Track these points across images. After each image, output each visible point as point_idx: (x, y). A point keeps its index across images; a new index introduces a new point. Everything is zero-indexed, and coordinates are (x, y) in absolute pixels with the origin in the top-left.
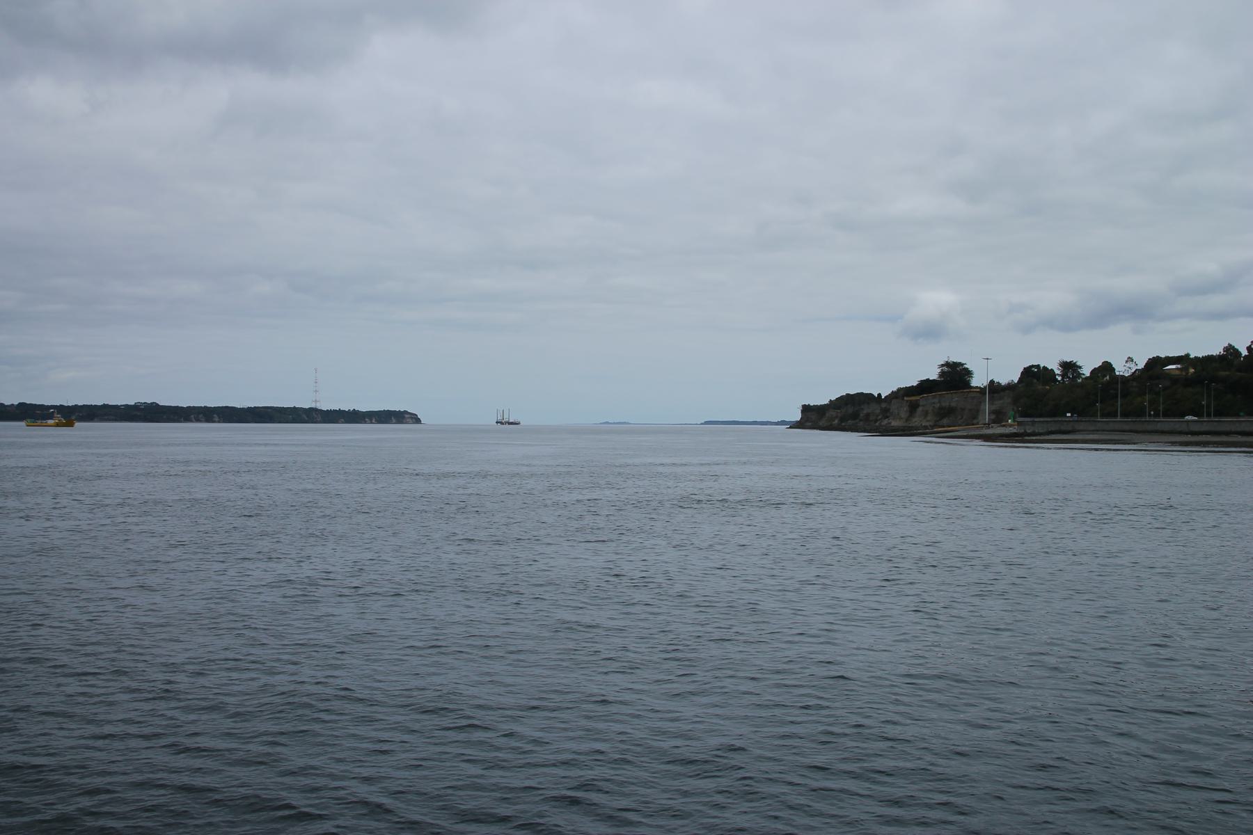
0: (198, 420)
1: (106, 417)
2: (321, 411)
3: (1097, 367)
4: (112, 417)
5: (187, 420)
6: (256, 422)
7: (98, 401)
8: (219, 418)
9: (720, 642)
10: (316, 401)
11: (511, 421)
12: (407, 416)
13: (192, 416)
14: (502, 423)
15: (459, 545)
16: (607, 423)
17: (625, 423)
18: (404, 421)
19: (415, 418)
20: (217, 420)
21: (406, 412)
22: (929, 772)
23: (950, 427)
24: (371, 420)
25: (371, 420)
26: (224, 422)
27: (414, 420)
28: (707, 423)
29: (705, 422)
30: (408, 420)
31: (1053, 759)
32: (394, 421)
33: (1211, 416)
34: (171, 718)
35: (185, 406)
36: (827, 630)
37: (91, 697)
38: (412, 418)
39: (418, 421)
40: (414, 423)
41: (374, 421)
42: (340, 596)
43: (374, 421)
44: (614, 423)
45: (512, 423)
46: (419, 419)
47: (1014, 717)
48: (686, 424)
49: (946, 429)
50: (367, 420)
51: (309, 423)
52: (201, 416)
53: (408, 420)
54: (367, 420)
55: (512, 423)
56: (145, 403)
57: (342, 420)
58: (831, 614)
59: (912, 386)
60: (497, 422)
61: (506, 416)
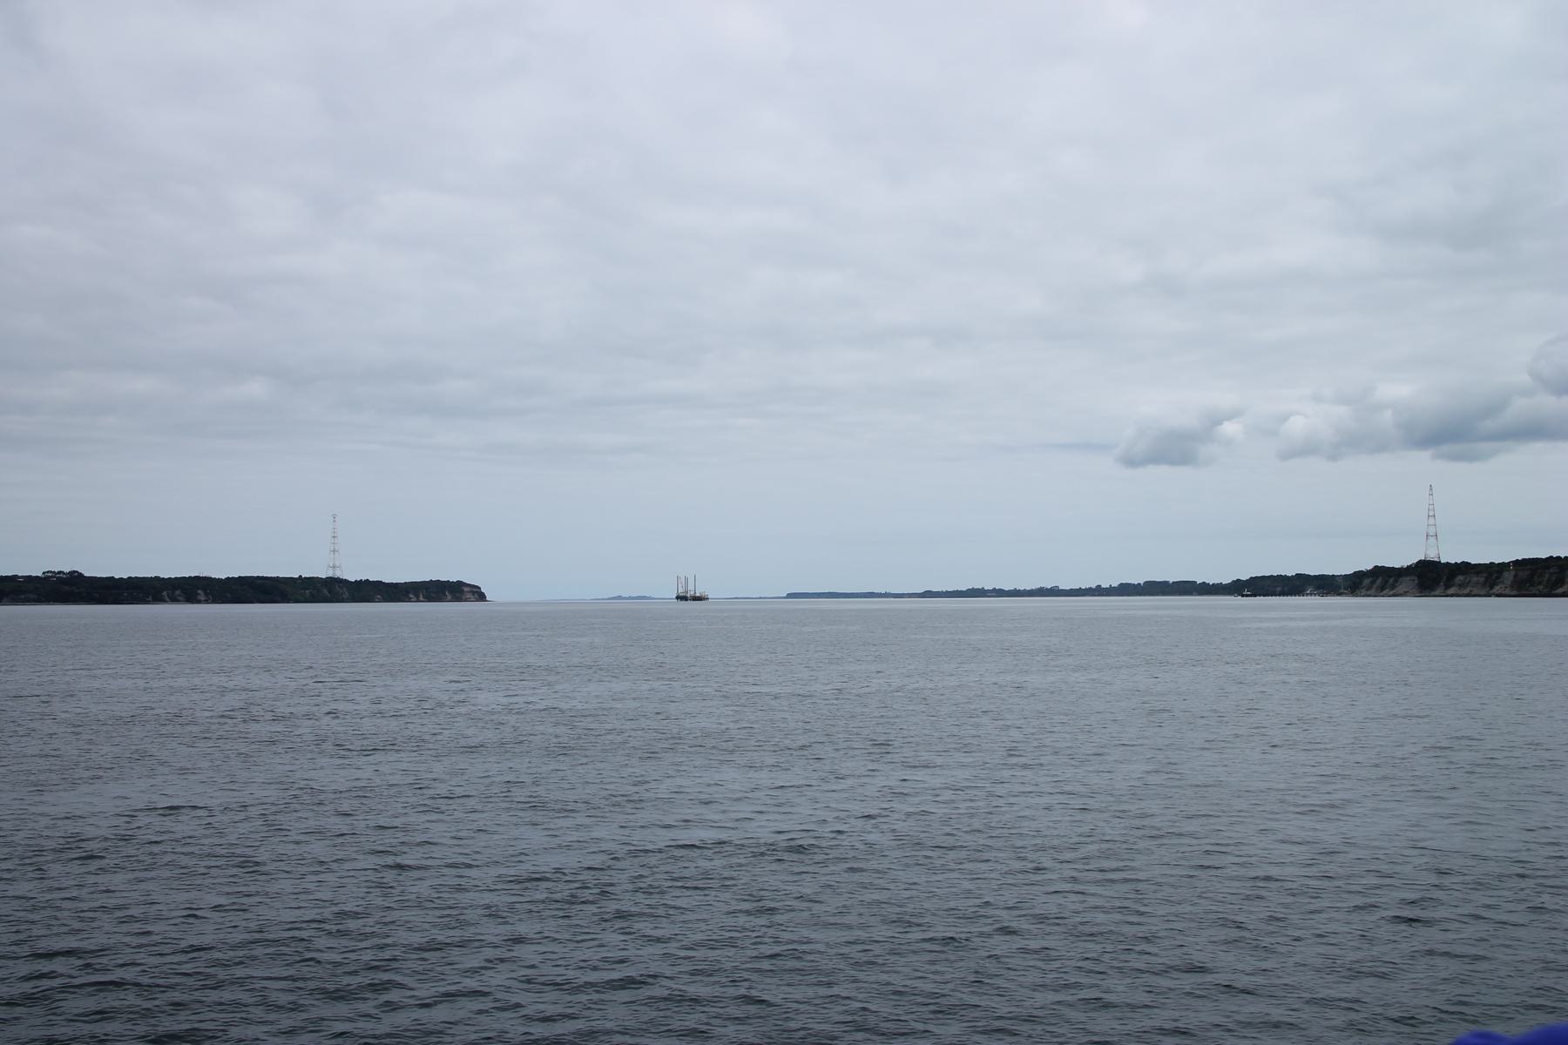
0: (174, 600)
1: (22, 596)
3: (371, 580)
4: (32, 596)
5: (158, 599)
6: (1128, 595)
8: (206, 594)
10: (334, 567)
11: (698, 595)
12: (466, 589)
13: (165, 593)
16: (620, 597)
18: (464, 598)
19: (477, 592)
20: (203, 598)
21: (460, 584)
22: (979, 1009)
24: (417, 597)
25: (417, 597)
26: (214, 601)
27: (477, 596)
28: (790, 596)
29: (788, 594)
31: (525, 797)
35: (117, 577)
36: (676, 792)
38: (473, 593)
39: (481, 597)
41: (421, 599)
43: (421, 599)
44: (630, 598)
46: (484, 594)
48: (760, 598)
52: (178, 592)
53: (468, 596)
56: (60, 572)
57: (379, 596)
60: (678, 598)
61: (691, 587)
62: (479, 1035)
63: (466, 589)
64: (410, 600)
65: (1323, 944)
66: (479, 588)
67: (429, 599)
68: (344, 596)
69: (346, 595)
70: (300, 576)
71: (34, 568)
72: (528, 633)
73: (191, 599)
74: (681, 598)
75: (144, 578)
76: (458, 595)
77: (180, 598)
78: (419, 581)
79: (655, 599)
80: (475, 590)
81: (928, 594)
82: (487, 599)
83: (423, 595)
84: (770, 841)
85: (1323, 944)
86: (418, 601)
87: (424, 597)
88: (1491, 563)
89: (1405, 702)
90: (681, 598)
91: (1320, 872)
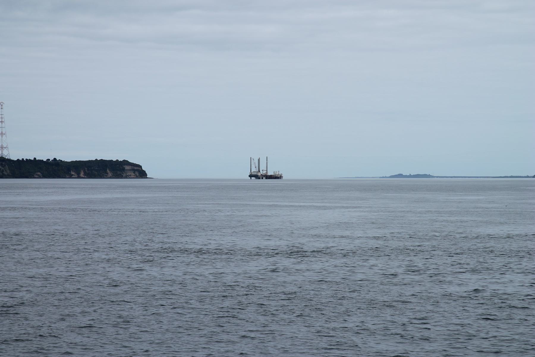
2: (9, 160)
5: (523, 178)
7: (44, 156)
9: (194, 352)
11: (270, 173)
12: (127, 168)
14: (257, 177)
15: (347, 299)
16: (400, 176)
17: (425, 176)
18: (124, 175)
19: (137, 170)
21: (125, 162)
30: (129, 174)
32: (110, 174)
35: (114, 160)
38: (134, 171)
40: (137, 177)
41: (82, 175)
43: (82, 175)
44: (410, 176)
47: (128, 355)
50: (73, 173)
51: (77, 178)
54: (73, 173)
57: (39, 173)
58: (102, 321)
60: (251, 176)
61: (263, 167)
62: (481, 316)
64: (71, 177)
65: (201, 309)
66: (141, 167)
68: (5, 173)
69: (7, 172)
70: (35, 158)
72: (530, 188)
73: (501, 178)
75: (76, 161)
77: (129, 173)
80: (136, 168)
81: (383, 177)
85: (201, 309)
86: (79, 177)
87: (85, 174)
88: (124, 161)
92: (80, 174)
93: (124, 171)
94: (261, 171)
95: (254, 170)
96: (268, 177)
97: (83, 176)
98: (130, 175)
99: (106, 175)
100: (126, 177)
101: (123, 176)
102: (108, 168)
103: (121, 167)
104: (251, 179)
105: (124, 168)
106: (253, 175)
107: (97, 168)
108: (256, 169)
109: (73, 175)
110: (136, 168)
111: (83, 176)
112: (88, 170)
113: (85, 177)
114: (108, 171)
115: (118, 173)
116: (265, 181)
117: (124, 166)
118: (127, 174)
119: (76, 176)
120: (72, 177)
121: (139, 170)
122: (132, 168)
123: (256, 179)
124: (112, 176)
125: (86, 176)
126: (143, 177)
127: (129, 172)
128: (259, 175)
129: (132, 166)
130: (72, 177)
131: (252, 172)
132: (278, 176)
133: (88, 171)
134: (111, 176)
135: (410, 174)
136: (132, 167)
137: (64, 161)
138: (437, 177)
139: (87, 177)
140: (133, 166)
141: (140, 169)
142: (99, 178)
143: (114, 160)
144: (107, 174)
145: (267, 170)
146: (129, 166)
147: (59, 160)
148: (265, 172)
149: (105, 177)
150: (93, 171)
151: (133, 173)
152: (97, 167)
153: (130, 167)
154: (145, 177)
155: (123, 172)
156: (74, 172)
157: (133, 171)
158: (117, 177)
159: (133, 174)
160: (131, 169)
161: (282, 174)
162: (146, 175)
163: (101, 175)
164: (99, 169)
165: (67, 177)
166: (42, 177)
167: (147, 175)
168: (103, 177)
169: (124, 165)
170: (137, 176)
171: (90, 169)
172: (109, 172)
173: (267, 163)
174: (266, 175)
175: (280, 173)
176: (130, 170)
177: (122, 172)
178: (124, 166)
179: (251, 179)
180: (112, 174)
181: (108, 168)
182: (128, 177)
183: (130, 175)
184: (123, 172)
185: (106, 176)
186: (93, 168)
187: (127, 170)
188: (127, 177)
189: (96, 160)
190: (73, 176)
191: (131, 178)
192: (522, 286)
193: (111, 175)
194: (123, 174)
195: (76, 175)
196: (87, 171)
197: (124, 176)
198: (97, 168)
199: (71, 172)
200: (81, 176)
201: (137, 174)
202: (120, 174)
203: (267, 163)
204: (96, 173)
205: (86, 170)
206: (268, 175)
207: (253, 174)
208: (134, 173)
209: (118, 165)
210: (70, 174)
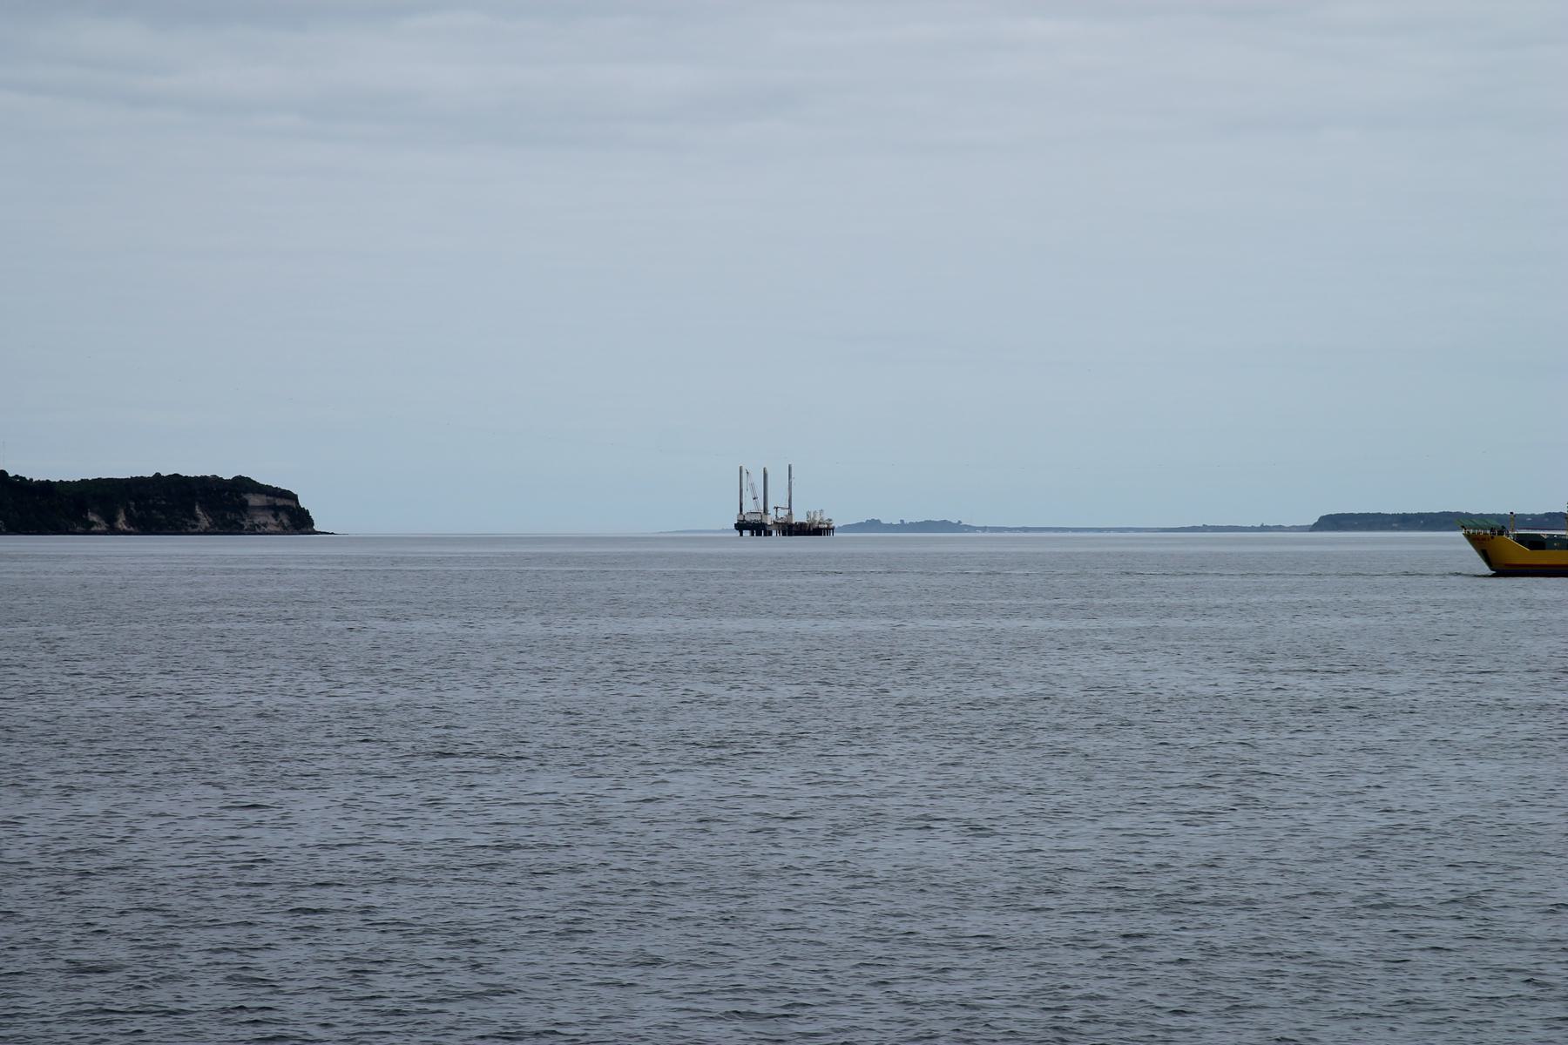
3: (164, 474)
11: (799, 518)
12: (254, 500)
14: (758, 528)
16: (874, 525)
18: (247, 524)
19: (285, 508)
21: (243, 485)
23: (1536, 529)
29: (1323, 519)
32: (205, 522)
33: (761, 535)
34: (1322, 927)
35: (231, 478)
37: (941, 887)
38: (275, 510)
39: (294, 518)
41: (121, 523)
42: (518, 758)
43: (121, 523)
44: (903, 527)
45: (791, 529)
49: (703, 550)
50: (93, 518)
51: (284, 534)
53: (260, 519)
54: (93, 518)
55: (791, 529)
59: (271, 486)
60: (741, 526)
61: (777, 498)
63: (254, 500)
64: (88, 530)
66: (294, 497)
67: (146, 525)
71: (1436, 509)
74: (752, 527)
75: (176, 477)
76: (230, 516)
78: (1436, 511)
79: (974, 529)
80: (280, 502)
82: (316, 528)
83: (129, 515)
84: (1006, 889)
86: (113, 530)
87: (130, 521)
89: (248, 637)
90: (752, 527)
91: (386, 912)
92: (116, 520)
93: (245, 512)
94: (771, 510)
95: (749, 507)
96: (794, 529)
97: (125, 527)
98: (265, 525)
99: (194, 523)
100: (254, 530)
101: (242, 526)
102: (197, 503)
103: (235, 499)
104: (741, 535)
105: (247, 501)
106: (748, 523)
107: (164, 503)
108: (757, 504)
109: (93, 523)
110: (280, 502)
111: (125, 527)
112: (138, 508)
113: (132, 529)
114: (198, 510)
115: (228, 517)
116: (778, 544)
117: (245, 497)
118: (256, 522)
119: (104, 528)
120: (93, 529)
121: (289, 506)
122: (268, 501)
123: (752, 535)
124: (212, 527)
125: (133, 526)
126: (304, 530)
127: (260, 513)
128: (769, 523)
129: (267, 496)
130: (93, 529)
131: (744, 512)
132: (821, 526)
133: (137, 511)
134: (206, 528)
135: (902, 521)
136: (269, 498)
137: (31, 480)
138: (984, 529)
139: (137, 531)
140: (270, 496)
141: (294, 505)
142: (173, 532)
143: (227, 475)
144: (197, 520)
145: (790, 508)
146: (259, 495)
147: (17, 476)
148: (782, 514)
149: (190, 529)
150: (154, 512)
151: (271, 517)
152: (165, 500)
153: (264, 497)
154: (310, 530)
155: (244, 515)
156: (97, 513)
157: (273, 512)
158: (226, 531)
159: (273, 521)
160: (265, 503)
161: (830, 520)
162: (311, 523)
163: (179, 523)
164: (171, 504)
165: (79, 529)
166: (4, 530)
167: (313, 524)
168: (183, 531)
169: (245, 493)
170: (285, 528)
171: (142, 503)
172: (201, 513)
173: (790, 483)
174: (786, 523)
175: (825, 519)
176: (263, 508)
177: (241, 515)
178: (245, 497)
179: (741, 535)
180: (211, 520)
181: (197, 503)
182: (258, 531)
183: (265, 525)
184: (244, 515)
185: (194, 527)
186: (151, 501)
187: (255, 508)
188: (255, 530)
189: (157, 475)
190: (95, 528)
191: (267, 534)
192: (944, 970)
193: (208, 525)
194: (244, 520)
195: (102, 522)
196: (135, 511)
197: (246, 527)
198: (164, 503)
199: (87, 515)
200: (120, 526)
201: (286, 521)
202: (235, 522)
203: (790, 483)
204: (163, 517)
205: (132, 509)
206: (794, 522)
207: (748, 519)
208: (276, 516)
209: (226, 494)
210: (87, 520)
